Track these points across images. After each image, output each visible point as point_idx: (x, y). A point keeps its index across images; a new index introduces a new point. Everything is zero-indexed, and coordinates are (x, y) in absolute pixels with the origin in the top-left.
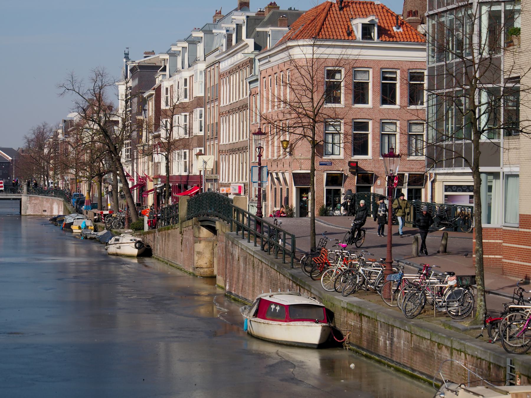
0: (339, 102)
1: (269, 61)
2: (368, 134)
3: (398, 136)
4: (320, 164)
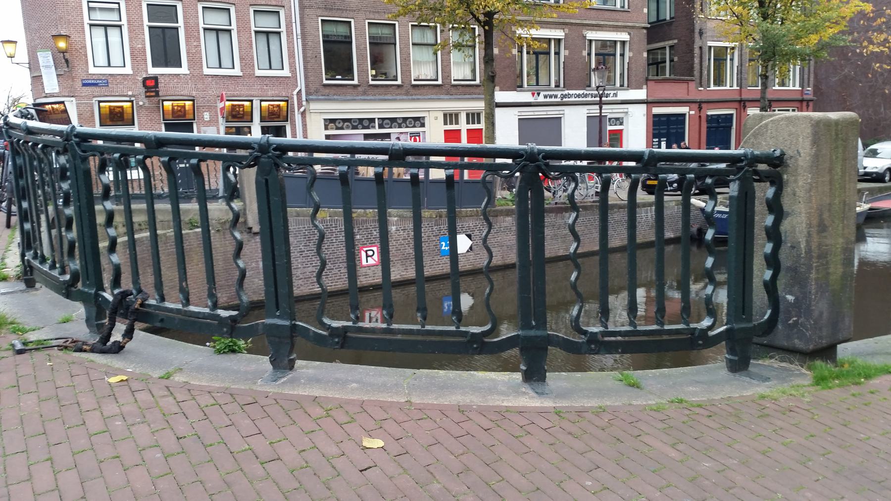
0: (179, 65)
1: (701, 48)
2: (177, 28)
3: (234, 34)
4: (84, 85)
